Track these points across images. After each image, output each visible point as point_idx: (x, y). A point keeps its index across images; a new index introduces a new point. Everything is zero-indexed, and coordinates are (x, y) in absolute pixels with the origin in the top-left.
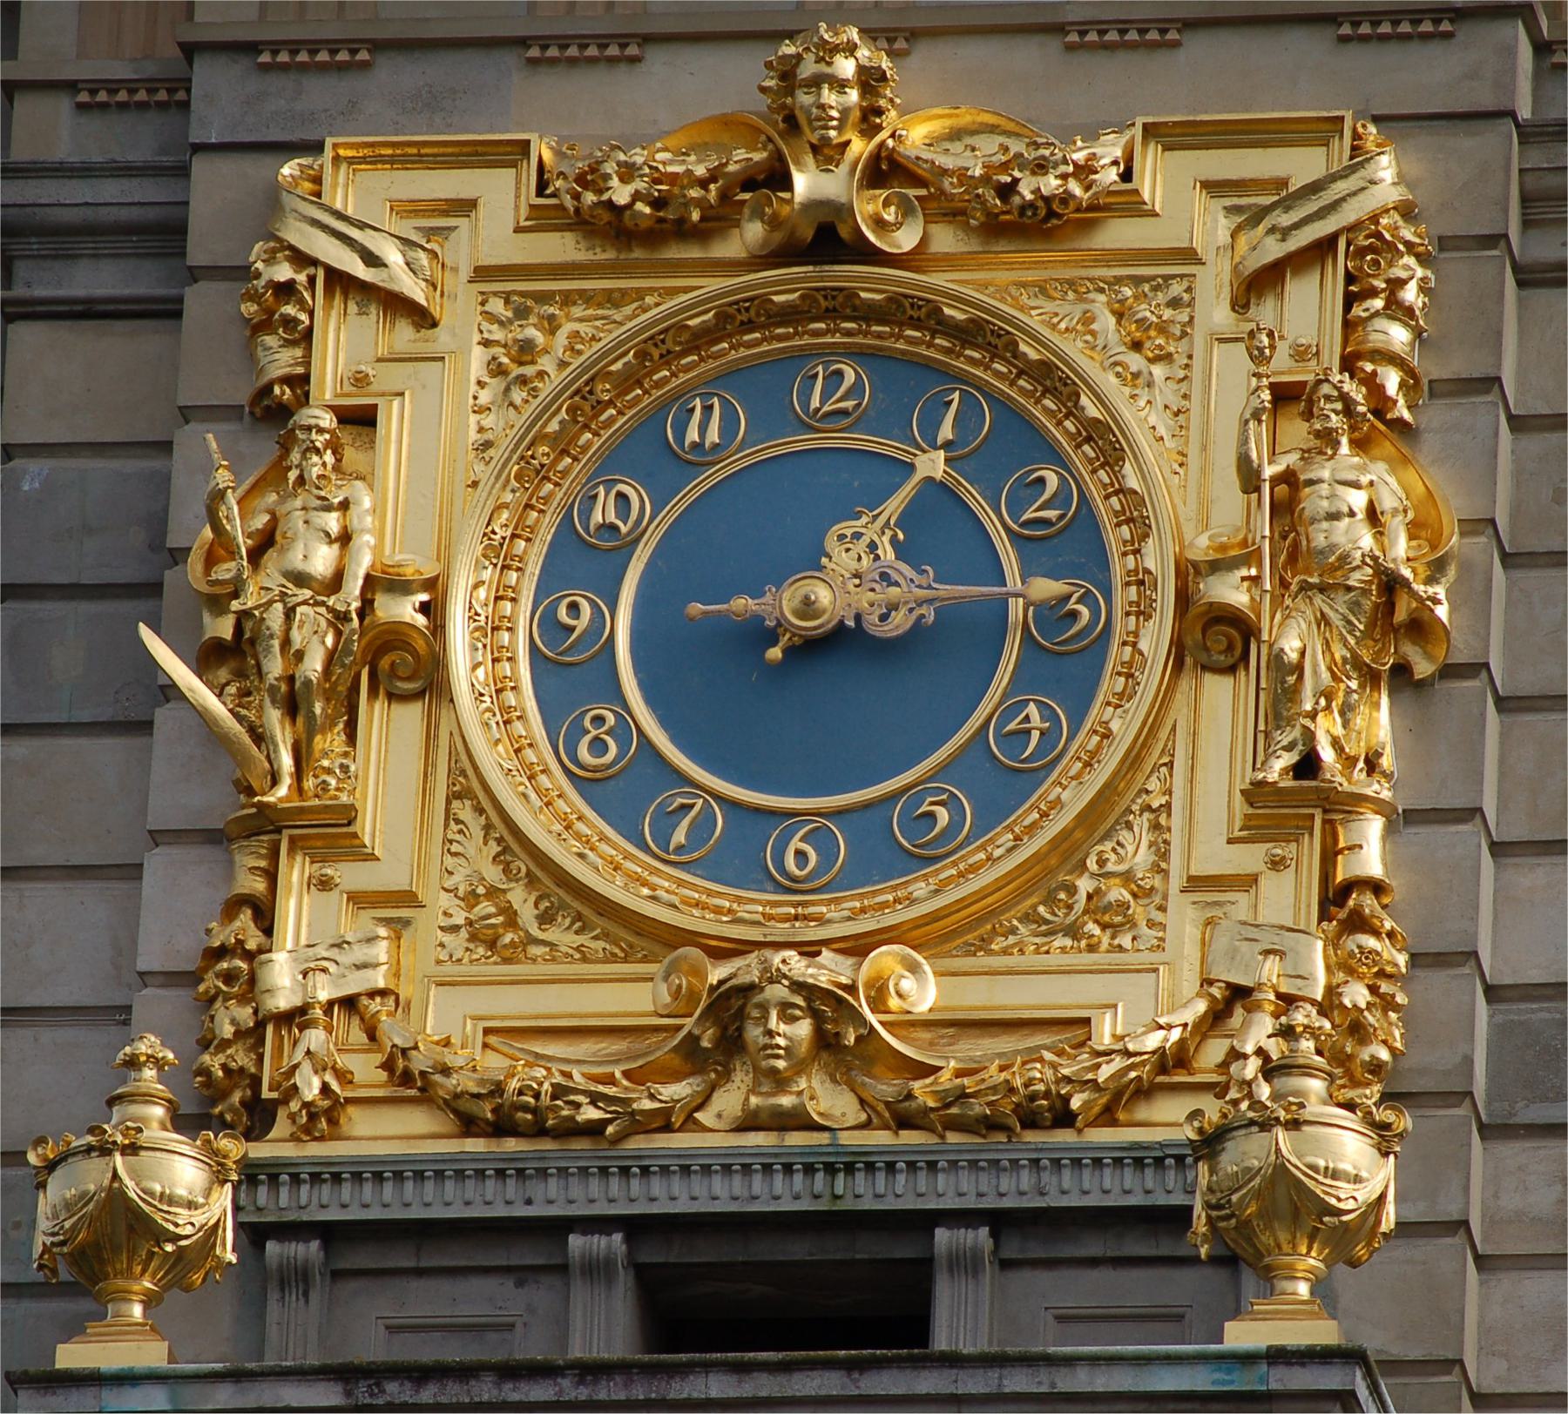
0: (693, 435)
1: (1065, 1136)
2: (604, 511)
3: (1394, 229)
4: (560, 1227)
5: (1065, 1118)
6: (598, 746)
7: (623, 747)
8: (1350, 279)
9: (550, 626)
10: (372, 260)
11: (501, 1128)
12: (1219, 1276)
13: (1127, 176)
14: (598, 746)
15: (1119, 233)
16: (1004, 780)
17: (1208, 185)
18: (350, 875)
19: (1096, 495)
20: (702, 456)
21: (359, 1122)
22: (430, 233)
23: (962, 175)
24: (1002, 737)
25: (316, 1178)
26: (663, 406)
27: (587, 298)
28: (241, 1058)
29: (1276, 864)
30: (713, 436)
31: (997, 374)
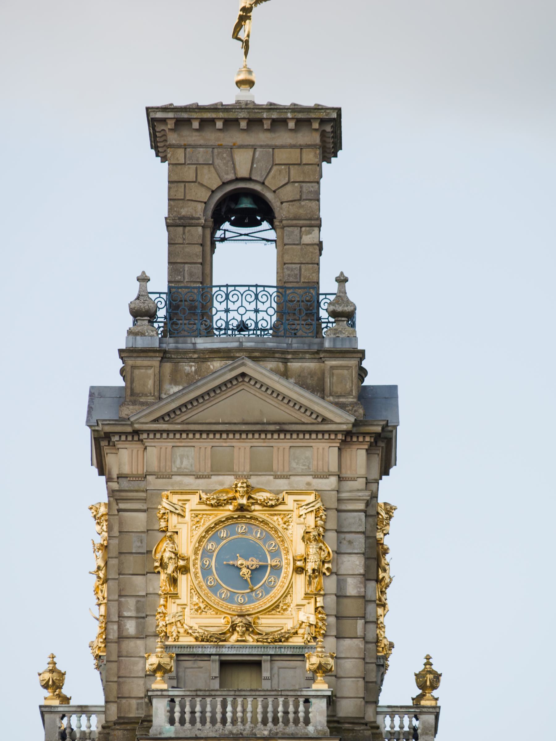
0: (222, 536)
1: (280, 644)
2: (210, 547)
3: (191, 366)
4: (210, 655)
5: (281, 641)
6: (211, 582)
7: (214, 582)
8: (316, 515)
9: (203, 565)
10: (176, 509)
11: (202, 641)
12: (375, 657)
13: (283, 500)
14: (211, 582)
15: (281, 507)
16: (267, 589)
17: (294, 501)
18: (178, 601)
19: (280, 546)
20: (223, 539)
21: (181, 639)
22: (183, 504)
23: (260, 500)
24: (268, 582)
25: (300, 648)
26: (218, 531)
27: (207, 514)
28: (164, 629)
29: (309, 603)
30: (225, 536)
31: (265, 527)
